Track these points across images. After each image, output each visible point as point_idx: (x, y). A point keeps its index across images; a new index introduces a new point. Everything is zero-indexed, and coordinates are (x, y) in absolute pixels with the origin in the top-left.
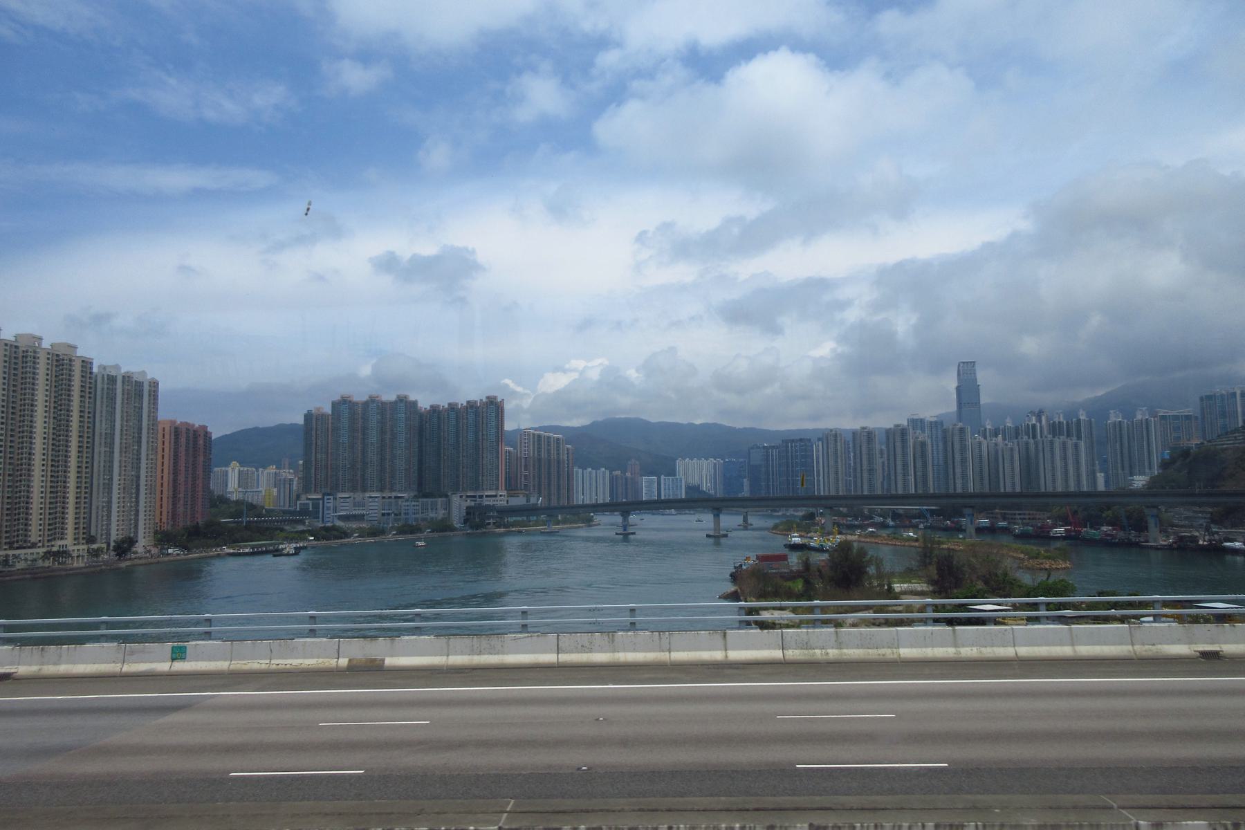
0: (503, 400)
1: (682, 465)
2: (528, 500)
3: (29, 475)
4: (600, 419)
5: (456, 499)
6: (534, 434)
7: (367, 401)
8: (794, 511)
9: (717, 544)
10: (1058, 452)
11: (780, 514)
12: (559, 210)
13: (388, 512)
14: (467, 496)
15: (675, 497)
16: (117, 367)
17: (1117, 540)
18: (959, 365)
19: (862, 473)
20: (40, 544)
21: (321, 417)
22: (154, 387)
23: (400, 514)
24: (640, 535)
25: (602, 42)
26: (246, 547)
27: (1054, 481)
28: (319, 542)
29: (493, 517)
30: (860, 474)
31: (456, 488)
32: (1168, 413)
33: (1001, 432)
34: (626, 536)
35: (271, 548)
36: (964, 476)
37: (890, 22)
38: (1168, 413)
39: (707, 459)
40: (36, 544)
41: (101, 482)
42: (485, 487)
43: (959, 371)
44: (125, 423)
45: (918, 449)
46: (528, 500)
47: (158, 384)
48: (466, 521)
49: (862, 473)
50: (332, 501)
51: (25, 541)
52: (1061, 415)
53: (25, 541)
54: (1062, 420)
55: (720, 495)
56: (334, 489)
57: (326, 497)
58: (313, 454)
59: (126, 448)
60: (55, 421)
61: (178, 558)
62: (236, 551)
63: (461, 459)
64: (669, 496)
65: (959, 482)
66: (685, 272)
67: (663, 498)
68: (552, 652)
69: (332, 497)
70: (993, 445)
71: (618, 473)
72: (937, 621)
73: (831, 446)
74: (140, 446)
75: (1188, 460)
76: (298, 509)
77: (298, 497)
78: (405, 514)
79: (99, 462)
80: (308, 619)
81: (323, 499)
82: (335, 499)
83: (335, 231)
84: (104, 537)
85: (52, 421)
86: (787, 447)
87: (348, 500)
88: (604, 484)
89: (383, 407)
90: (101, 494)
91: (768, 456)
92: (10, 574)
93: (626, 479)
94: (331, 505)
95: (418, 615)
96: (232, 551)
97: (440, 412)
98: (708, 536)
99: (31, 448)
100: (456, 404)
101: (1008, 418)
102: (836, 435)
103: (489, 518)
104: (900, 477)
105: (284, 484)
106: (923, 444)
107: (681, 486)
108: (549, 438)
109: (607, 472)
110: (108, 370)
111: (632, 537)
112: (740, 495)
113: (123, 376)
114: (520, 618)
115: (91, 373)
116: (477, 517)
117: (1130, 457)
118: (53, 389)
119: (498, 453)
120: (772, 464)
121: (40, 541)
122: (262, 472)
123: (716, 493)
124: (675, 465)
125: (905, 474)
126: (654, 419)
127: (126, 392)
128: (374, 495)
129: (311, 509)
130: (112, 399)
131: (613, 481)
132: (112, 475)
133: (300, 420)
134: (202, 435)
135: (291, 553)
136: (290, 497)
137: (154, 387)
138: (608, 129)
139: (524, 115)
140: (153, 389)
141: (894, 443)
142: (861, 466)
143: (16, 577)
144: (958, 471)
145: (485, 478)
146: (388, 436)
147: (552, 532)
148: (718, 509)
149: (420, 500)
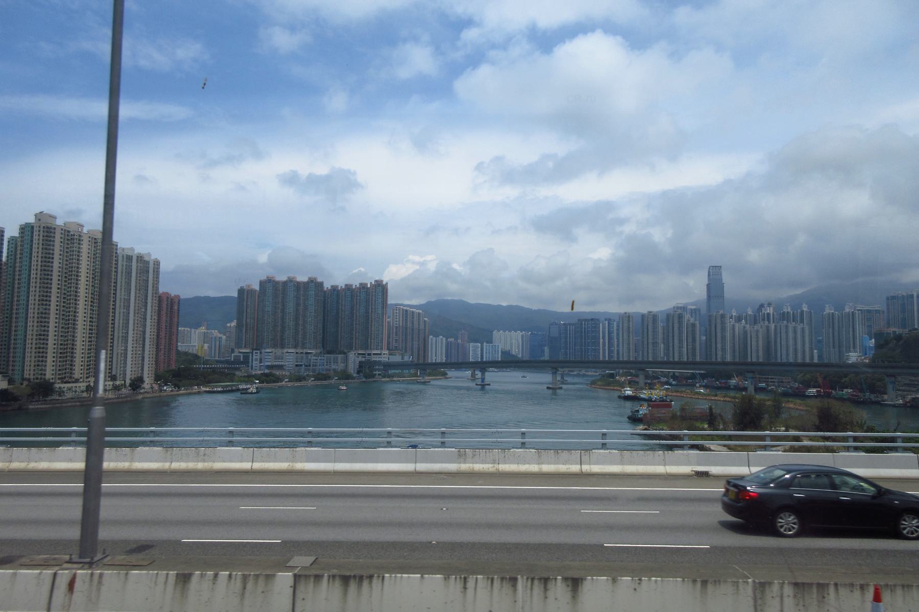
0: (387, 283)
1: (497, 335)
2: (403, 358)
3: (74, 328)
4: (433, 300)
5: (352, 355)
6: (403, 309)
7: (287, 281)
8: (586, 371)
9: (555, 394)
10: (791, 335)
11: (575, 373)
12: (422, 144)
13: (301, 363)
14: (359, 354)
15: (494, 359)
16: (132, 249)
17: (862, 400)
18: (709, 269)
19: (648, 345)
20: (81, 380)
21: (251, 292)
22: (157, 265)
23: (310, 366)
24: (494, 386)
25: (467, 23)
26: (217, 387)
27: (787, 354)
28: (263, 385)
29: (379, 370)
30: (646, 346)
31: (350, 348)
32: (863, 308)
33: (744, 318)
34: (483, 386)
35: (234, 388)
36: (724, 350)
37: (683, 16)
38: (863, 308)
39: (510, 331)
40: (79, 380)
41: (121, 334)
42: (372, 347)
43: (709, 272)
44: (138, 292)
45: (690, 329)
46: (403, 358)
47: (160, 263)
48: (358, 372)
49: (648, 345)
50: (259, 354)
51: (71, 378)
52: (789, 307)
53: (71, 378)
54: (789, 310)
55: (526, 358)
56: (258, 347)
57: (254, 352)
58: (245, 319)
59: (138, 310)
60: (93, 288)
61: (173, 393)
62: (211, 389)
63: (354, 326)
64: (489, 358)
65: (720, 353)
66: (510, 192)
67: (484, 360)
68: (577, 464)
69: (258, 352)
70: (742, 327)
71: (452, 340)
72: (856, 449)
73: (626, 325)
74: (146, 309)
75: (901, 343)
76: (232, 360)
77: (233, 351)
78: (313, 365)
79: (119, 320)
80: (521, 434)
81: (252, 353)
82: (261, 353)
83: (258, 155)
84: (122, 376)
85: (91, 288)
86: (581, 324)
87: (271, 354)
88: (441, 348)
89: (298, 286)
90: (120, 344)
91: (566, 330)
92: (63, 402)
93: (458, 344)
94: (258, 357)
95: (310, 432)
96: (208, 389)
97: (338, 291)
98: (548, 388)
99: (75, 308)
100: (351, 285)
101: (749, 308)
102: (629, 317)
103: (376, 370)
104: (676, 349)
105: (215, 341)
106: (693, 325)
107: (498, 351)
108: (413, 312)
109: (444, 339)
110: (125, 251)
111: (487, 387)
112: (542, 359)
113: (138, 256)
114: (520, 437)
115: (116, 253)
116: (367, 369)
117: (839, 339)
118: (92, 264)
119: (383, 322)
120: (570, 336)
121: (81, 378)
122: (195, 332)
123: (522, 356)
124: (492, 335)
125: (681, 347)
126: (472, 301)
127: (139, 268)
128: (290, 351)
129: (242, 360)
130: (129, 274)
131: (448, 346)
132: (128, 330)
133: (235, 294)
134: (177, 302)
135: (254, 392)
136: (219, 350)
137: (157, 265)
138: (465, 85)
139: (404, 73)
140: (156, 266)
141: (673, 324)
142: (648, 341)
143: (70, 404)
144: (719, 346)
145: (372, 341)
146: (301, 308)
147: (425, 382)
148: (556, 368)
149: (326, 355)
